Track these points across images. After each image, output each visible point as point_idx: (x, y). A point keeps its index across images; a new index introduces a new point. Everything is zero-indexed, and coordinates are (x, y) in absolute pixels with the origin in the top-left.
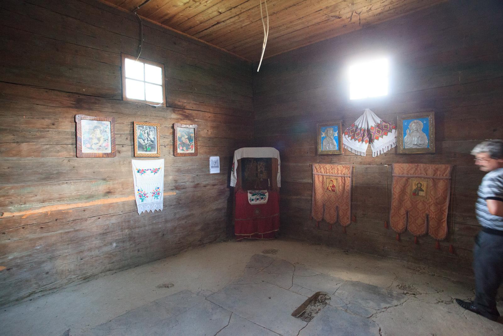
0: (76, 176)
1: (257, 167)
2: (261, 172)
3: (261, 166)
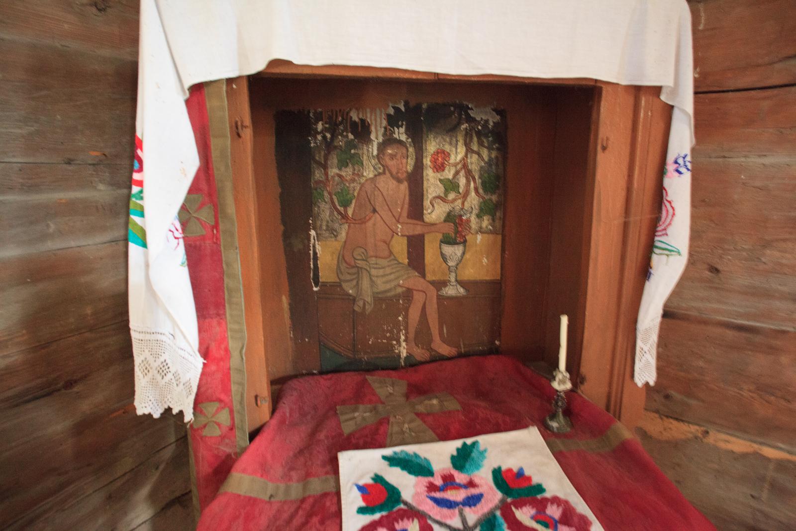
0: (100, 140)
1: (415, 180)
2: (456, 230)
3: (449, 174)
